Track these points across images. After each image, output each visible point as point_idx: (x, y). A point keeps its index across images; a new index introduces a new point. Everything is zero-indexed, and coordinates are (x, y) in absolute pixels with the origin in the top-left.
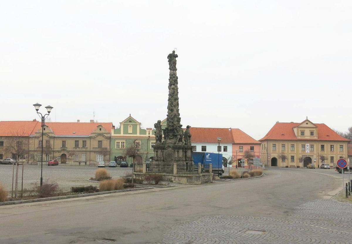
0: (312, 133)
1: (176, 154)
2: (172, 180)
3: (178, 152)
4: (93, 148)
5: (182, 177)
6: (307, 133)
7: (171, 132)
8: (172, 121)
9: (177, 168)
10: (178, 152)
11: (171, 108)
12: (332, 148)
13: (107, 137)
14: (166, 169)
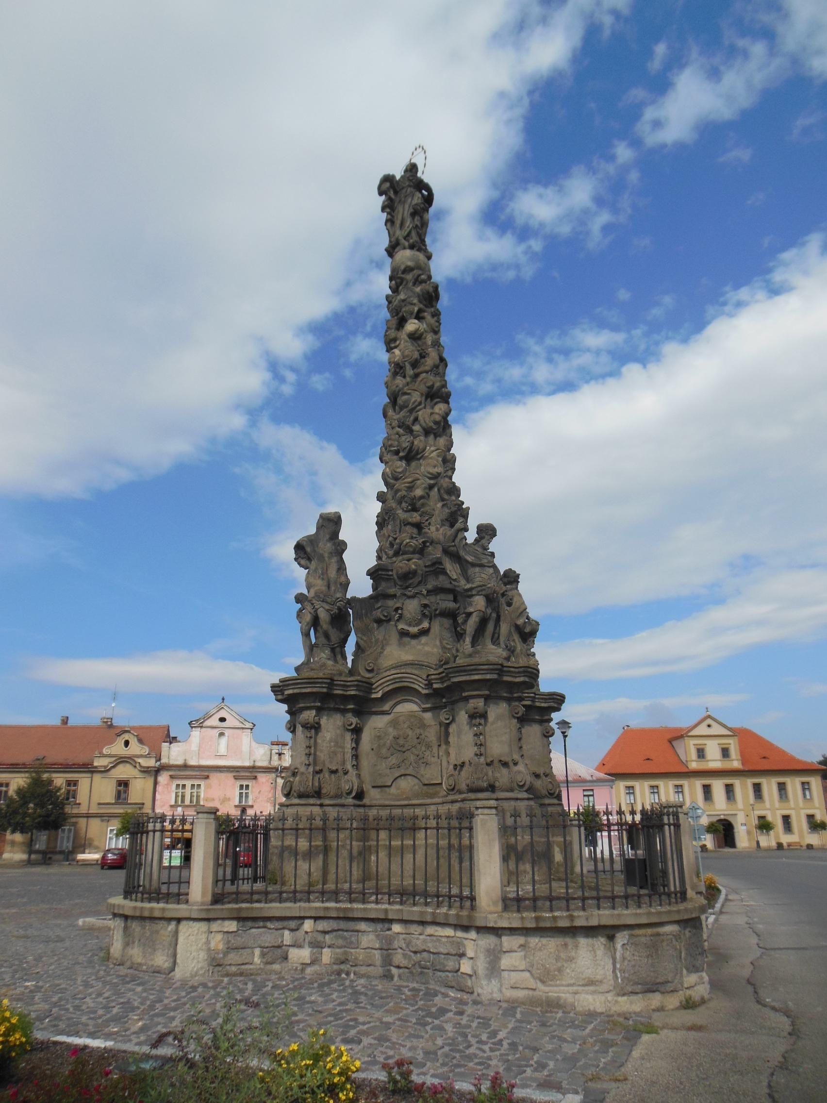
0: (725, 752)
1: (468, 736)
2: (466, 967)
3: (478, 717)
4: (99, 804)
5: (573, 931)
6: (713, 750)
7: (411, 592)
8: (415, 517)
9: (510, 853)
10: (478, 717)
11: (405, 441)
12: (807, 793)
13: (144, 767)
14: (379, 861)
